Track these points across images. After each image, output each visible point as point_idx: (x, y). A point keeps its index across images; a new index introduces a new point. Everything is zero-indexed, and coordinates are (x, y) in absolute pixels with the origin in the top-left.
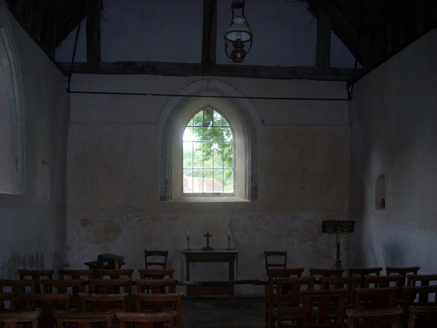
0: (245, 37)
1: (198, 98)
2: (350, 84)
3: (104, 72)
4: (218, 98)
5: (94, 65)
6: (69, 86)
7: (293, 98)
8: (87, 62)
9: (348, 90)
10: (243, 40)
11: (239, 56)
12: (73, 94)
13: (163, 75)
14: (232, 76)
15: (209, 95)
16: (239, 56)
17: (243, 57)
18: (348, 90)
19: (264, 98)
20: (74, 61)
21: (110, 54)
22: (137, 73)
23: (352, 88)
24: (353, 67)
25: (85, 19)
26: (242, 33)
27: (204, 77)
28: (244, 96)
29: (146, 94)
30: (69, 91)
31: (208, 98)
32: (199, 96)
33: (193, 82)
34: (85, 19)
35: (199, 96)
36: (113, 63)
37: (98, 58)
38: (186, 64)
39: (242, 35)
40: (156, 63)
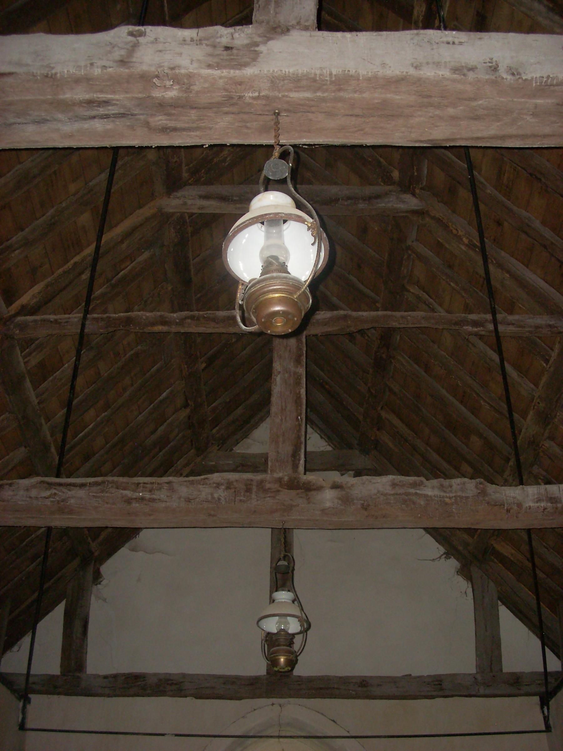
0: (294, 626)
1: (262, 739)
2: (545, 701)
3: (88, 693)
4: (300, 739)
5: (72, 679)
6: (24, 719)
7: (442, 733)
8: (59, 673)
9: (543, 712)
10: (291, 631)
11: (282, 660)
12: (33, 733)
13: (196, 698)
14: (323, 697)
15: (283, 734)
16: (282, 660)
17: (292, 663)
18: (543, 712)
19: (385, 737)
20: (32, 672)
21: (101, 660)
22: (149, 695)
23: (548, 709)
24: (25, 672)
25: (64, 602)
26: (288, 618)
27: (274, 700)
28: (348, 735)
29: (177, 735)
30: (22, 727)
31: (281, 740)
32: (268, 737)
33: (255, 710)
34: (64, 602)
35: (268, 737)
36: (105, 677)
37: (81, 666)
38: (238, 678)
39: (289, 623)
40: (184, 675)
